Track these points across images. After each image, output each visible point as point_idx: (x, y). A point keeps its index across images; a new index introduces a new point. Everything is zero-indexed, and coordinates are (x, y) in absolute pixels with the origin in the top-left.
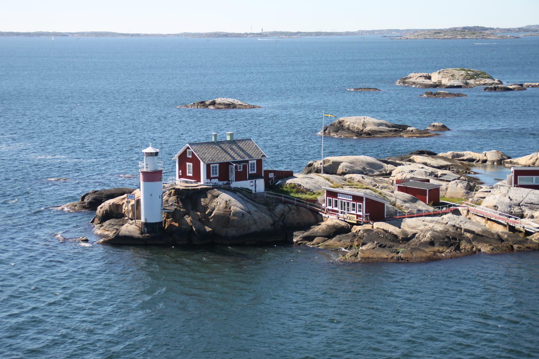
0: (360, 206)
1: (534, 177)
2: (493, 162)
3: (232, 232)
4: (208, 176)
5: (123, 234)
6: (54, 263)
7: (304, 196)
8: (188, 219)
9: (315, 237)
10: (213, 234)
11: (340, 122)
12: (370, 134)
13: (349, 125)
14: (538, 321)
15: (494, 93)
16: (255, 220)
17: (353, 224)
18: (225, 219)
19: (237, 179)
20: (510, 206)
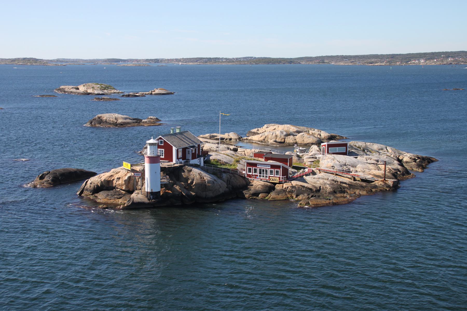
0: (277, 172)
1: (337, 148)
2: (236, 139)
3: (210, 194)
4: (178, 158)
5: (137, 201)
6: (363, 237)
7: (224, 167)
8: (177, 188)
9: (259, 194)
10: (196, 197)
11: (99, 118)
12: (122, 125)
13: (106, 119)
14: (466, 240)
15: (128, 98)
16: (219, 185)
17: (275, 184)
18: (202, 186)
19: (193, 159)
20: (341, 166)
